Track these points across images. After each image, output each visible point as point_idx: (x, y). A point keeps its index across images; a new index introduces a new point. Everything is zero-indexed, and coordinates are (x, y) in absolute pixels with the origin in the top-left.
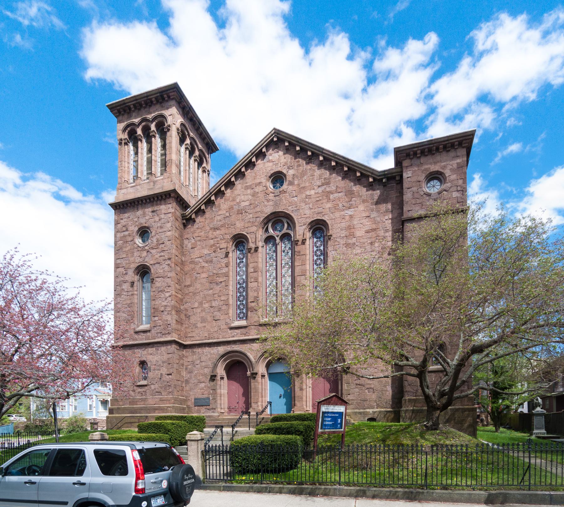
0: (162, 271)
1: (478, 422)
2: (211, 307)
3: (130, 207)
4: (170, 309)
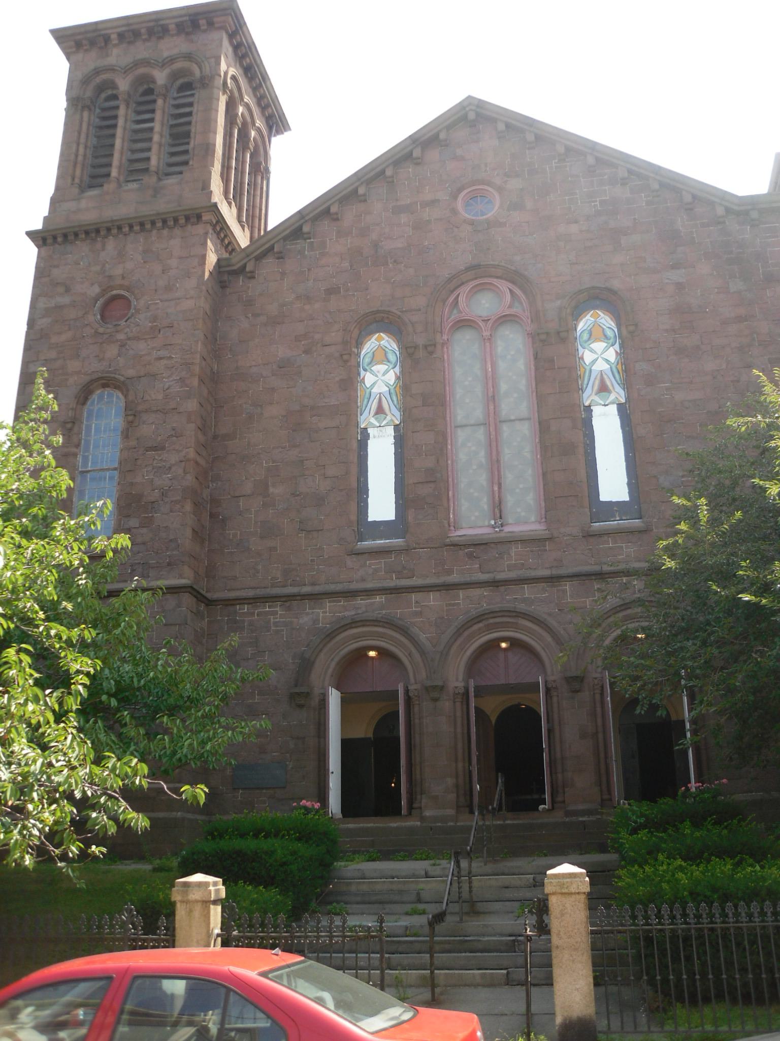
0: (160, 397)
1: (233, 927)
2: (293, 495)
3: (83, 240)
4: (179, 498)
